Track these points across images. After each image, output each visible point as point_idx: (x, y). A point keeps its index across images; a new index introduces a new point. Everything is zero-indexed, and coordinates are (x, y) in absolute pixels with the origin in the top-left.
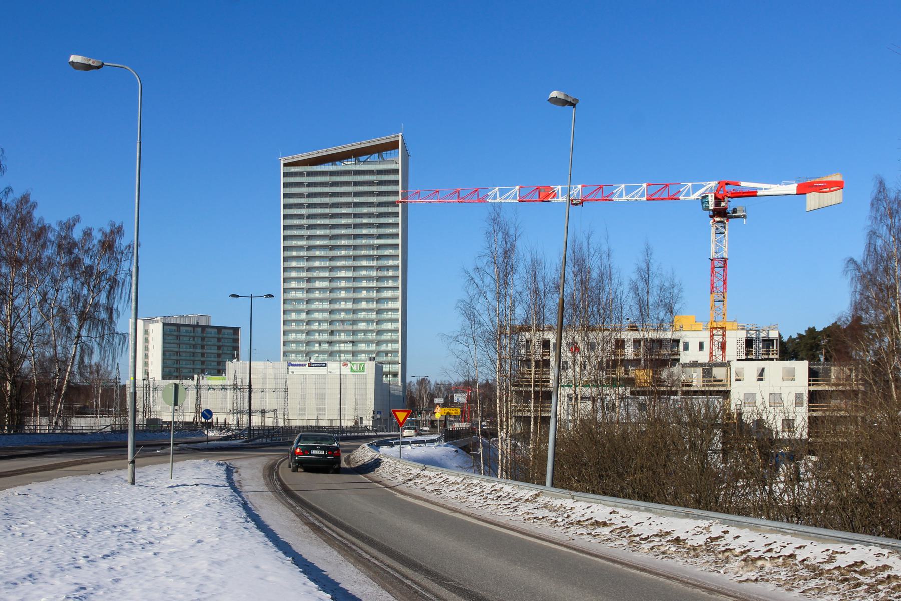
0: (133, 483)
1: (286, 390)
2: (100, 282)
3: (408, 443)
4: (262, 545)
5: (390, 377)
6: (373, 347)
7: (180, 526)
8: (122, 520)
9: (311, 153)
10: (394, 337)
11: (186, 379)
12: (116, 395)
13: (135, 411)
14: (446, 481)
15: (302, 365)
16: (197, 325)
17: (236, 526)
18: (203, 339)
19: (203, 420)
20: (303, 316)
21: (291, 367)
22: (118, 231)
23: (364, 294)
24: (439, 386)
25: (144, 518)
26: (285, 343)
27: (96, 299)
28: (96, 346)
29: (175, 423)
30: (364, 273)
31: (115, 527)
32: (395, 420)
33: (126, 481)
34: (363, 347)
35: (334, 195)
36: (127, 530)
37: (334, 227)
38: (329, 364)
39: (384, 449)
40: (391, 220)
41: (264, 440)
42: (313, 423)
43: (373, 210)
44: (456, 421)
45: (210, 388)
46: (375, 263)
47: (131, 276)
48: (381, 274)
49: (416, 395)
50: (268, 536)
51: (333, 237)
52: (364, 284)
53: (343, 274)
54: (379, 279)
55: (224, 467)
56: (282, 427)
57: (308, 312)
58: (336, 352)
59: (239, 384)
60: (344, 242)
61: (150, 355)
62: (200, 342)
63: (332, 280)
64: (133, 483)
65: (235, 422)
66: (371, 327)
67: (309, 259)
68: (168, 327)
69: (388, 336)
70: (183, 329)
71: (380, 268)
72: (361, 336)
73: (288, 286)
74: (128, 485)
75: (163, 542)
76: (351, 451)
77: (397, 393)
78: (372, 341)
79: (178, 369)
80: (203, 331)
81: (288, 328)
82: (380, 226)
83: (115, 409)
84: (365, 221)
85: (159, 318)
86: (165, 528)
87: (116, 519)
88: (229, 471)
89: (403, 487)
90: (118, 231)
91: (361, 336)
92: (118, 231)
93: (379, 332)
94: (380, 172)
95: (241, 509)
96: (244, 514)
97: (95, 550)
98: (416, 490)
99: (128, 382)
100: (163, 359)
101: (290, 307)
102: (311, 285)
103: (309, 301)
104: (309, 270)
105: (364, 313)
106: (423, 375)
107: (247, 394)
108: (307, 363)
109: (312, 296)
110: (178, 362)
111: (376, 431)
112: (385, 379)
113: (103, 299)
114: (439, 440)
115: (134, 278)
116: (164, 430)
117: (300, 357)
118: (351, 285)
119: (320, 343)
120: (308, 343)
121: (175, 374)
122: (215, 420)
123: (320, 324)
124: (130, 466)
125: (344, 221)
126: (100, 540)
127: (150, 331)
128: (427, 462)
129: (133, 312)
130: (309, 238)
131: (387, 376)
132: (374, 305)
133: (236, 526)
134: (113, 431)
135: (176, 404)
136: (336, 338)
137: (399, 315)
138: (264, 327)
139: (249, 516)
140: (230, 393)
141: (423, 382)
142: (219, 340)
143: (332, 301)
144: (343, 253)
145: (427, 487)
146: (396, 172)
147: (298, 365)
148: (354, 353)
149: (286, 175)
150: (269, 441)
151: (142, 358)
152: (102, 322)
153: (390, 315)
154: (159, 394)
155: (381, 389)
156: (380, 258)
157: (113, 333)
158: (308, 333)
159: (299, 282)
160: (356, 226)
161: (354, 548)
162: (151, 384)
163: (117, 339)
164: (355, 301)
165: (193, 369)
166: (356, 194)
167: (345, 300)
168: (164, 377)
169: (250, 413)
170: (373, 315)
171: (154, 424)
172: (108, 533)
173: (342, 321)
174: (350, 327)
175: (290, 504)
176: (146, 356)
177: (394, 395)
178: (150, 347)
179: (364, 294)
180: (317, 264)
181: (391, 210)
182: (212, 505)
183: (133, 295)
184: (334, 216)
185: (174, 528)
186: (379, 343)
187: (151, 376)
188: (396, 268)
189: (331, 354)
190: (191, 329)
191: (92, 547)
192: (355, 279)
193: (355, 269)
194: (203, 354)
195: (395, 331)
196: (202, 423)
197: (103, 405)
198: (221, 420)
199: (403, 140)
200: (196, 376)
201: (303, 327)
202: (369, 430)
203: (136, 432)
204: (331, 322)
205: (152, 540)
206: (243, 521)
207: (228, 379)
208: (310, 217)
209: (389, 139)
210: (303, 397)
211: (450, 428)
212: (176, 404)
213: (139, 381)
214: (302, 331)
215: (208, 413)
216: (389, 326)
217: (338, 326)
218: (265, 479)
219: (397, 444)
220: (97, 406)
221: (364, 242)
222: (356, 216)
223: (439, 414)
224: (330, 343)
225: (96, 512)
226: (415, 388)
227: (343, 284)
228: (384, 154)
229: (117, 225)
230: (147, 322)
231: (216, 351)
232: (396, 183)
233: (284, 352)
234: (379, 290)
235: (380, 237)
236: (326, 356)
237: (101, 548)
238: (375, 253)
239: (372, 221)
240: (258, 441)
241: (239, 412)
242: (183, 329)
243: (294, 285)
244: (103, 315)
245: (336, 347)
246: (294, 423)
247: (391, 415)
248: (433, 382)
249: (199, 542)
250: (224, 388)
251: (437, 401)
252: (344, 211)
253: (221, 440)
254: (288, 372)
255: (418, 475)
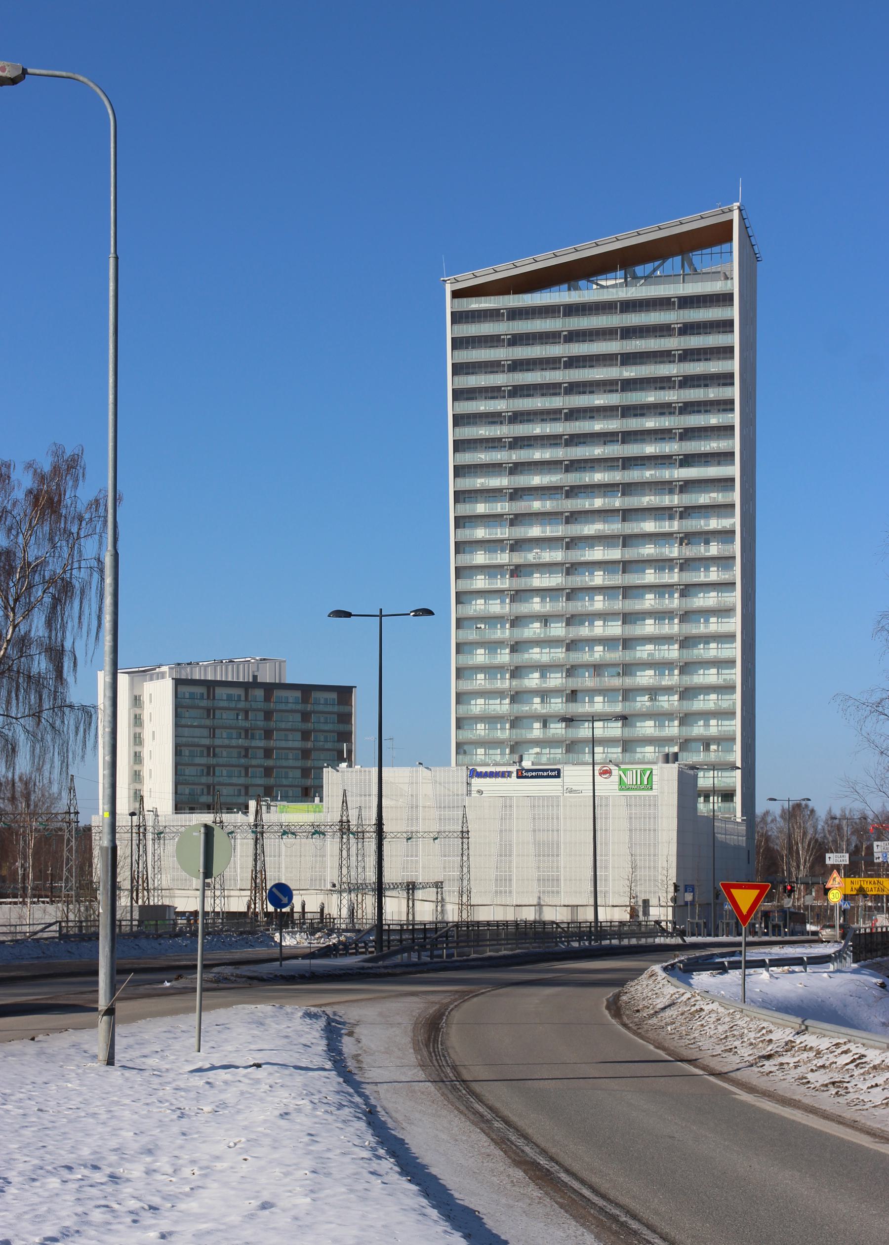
0: (110, 1061)
1: (464, 834)
2: (30, 587)
3: (761, 964)
4: (414, 1216)
5: (716, 802)
6: (673, 729)
7: (219, 1166)
8: (85, 1152)
9: (518, 262)
10: (725, 705)
11: (230, 810)
12: (69, 852)
13: (114, 887)
14: (859, 1061)
15: (503, 775)
16: (255, 684)
17: (351, 1169)
18: (268, 715)
19: (271, 908)
20: (504, 657)
21: (475, 781)
22: (69, 468)
23: (649, 601)
24: (835, 824)
25: (136, 1146)
26: (460, 723)
27: (23, 629)
28: (21, 737)
29: (206, 914)
30: (648, 550)
31: (69, 1168)
32: (728, 907)
33: (95, 1057)
34: (647, 728)
35: (573, 362)
36: (99, 1177)
37: (574, 440)
38: (568, 771)
39: (703, 979)
40: (714, 420)
41: (414, 958)
42: (529, 915)
43: (671, 396)
44: (880, 910)
45: (286, 832)
46: (675, 526)
47: (102, 571)
48: (690, 552)
49: (779, 844)
50: (426, 1193)
51: (573, 466)
52: (650, 576)
53: (598, 554)
54: (686, 564)
55: (322, 1023)
56: (457, 925)
57: (516, 647)
58: (584, 741)
59: (353, 822)
60: (599, 477)
61: (145, 755)
62: (261, 724)
63: (571, 568)
64: (110, 1061)
65: (345, 912)
66: (666, 681)
67: (516, 520)
68: (185, 690)
69: (709, 702)
70: (220, 692)
71: (687, 538)
72: (643, 702)
73: (468, 559)
74: (99, 1065)
75: (182, 1206)
76: (621, 983)
77: (732, 840)
78: (668, 716)
79: (210, 788)
80: (267, 698)
81: (467, 686)
82: (688, 434)
83: (67, 884)
84: (650, 423)
85: (165, 669)
86: (186, 1172)
87: (73, 1149)
88: (333, 1032)
89: (752, 1076)
90: (69, 467)
91: (643, 702)
92: (69, 468)
93: (687, 693)
94: (687, 302)
95: (362, 1125)
96: (370, 1139)
97: (26, 1225)
98: (785, 1082)
99: (98, 819)
100: (177, 784)
101: (471, 635)
102: (522, 583)
103: (516, 621)
104: (517, 545)
105: (650, 647)
106: (797, 796)
107: (371, 845)
108: (514, 769)
109: (524, 608)
110: (210, 770)
111: (682, 934)
112: (702, 807)
113: (37, 626)
114: (838, 956)
115: (108, 580)
116: (181, 934)
117: (496, 755)
118: (618, 579)
119: (545, 721)
120: (516, 722)
121: (204, 799)
122: (298, 908)
123: (543, 676)
124: (103, 1022)
125: (598, 426)
126: (36, 1200)
127: (145, 698)
128: (809, 1012)
129: (108, 659)
130: (516, 468)
131: (707, 797)
132: (674, 628)
133: (351, 1169)
134: (64, 937)
135: (208, 873)
136: (584, 707)
137: (735, 651)
138: (409, 684)
139: (381, 1143)
140: (332, 844)
141: (797, 812)
142: (305, 716)
143: (571, 620)
144: (598, 503)
145: (811, 1076)
146: (725, 299)
147: (491, 775)
148: (627, 745)
149: (458, 317)
150: (425, 958)
151: (131, 759)
152: (35, 681)
153: (713, 651)
154: (170, 847)
155: (693, 831)
156: (687, 512)
157: (62, 707)
158: (516, 697)
159: (492, 576)
160: (627, 437)
161: (634, 1225)
162: (150, 823)
163: (70, 718)
164: (627, 618)
165: (247, 788)
166: (628, 359)
167: (604, 616)
168: (178, 808)
169: (380, 890)
170: (672, 652)
171: (156, 917)
172: (54, 1183)
173: (598, 668)
174: (617, 682)
175: (476, 1113)
176: (137, 758)
177: (725, 846)
178: (147, 735)
179: (649, 601)
180: (535, 531)
181: (712, 393)
182: (294, 1115)
183: (107, 618)
184: (573, 414)
185: (207, 1172)
186: (686, 719)
187: (148, 806)
188: (726, 535)
189: (572, 746)
190: (240, 692)
191: (19, 1217)
192: (626, 566)
193: (627, 540)
194: (268, 753)
195: (727, 689)
196: (267, 914)
197: (40, 875)
198: (313, 907)
199: (742, 219)
200: (252, 804)
201: (504, 683)
202: (664, 931)
203: (115, 938)
204: (571, 671)
205: (156, 1200)
206: (366, 1154)
207: (327, 810)
208: (517, 417)
209: (708, 218)
210: (505, 852)
211: (862, 926)
212: (208, 873)
213: (123, 819)
214: (500, 694)
215: (281, 893)
216: (711, 677)
217: (588, 681)
218: (417, 1050)
219: (735, 965)
220: (25, 877)
221: (648, 474)
222: (627, 411)
223: (837, 891)
224: (569, 720)
225: (27, 1132)
226: (776, 828)
227: (598, 579)
228: (696, 257)
229: (68, 453)
230: (137, 679)
231: (298, 744)
232: (726, 326)
233: (459, 745)
234: (686, 590)
235: (687, 460)
236: (558, 752)
237: (39, 1219)
238: (674, 500)
239: (665, 422)
240: (398, 959)
241: (356, 888)
242: (220, 692)
243: (480, 582)
244: (41, 664)
245: (584, 731)
246: (483, 915)
247: (717, 895)
248: (822, 814)
249: (265, 1206)
250: (317, 832)
251: (831, 859)
252: (599, 400)
253: (311, 955)
254: (469, 793)
255: (789, 1046)
